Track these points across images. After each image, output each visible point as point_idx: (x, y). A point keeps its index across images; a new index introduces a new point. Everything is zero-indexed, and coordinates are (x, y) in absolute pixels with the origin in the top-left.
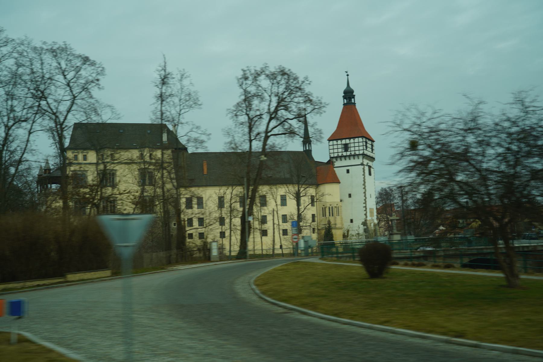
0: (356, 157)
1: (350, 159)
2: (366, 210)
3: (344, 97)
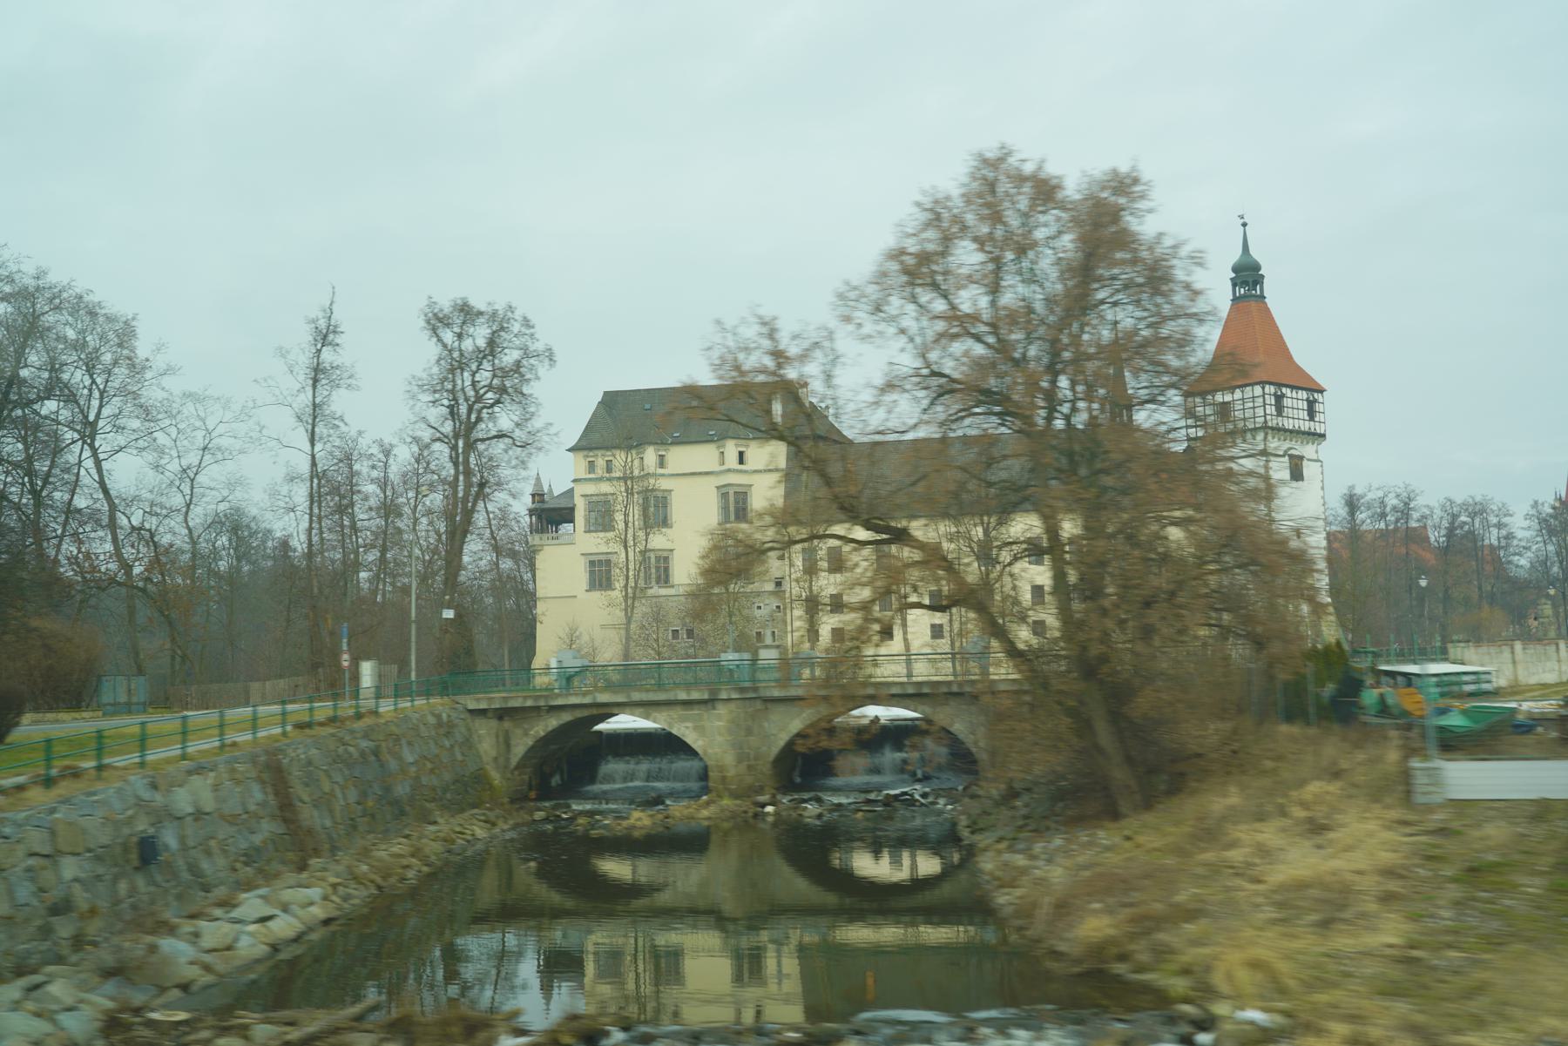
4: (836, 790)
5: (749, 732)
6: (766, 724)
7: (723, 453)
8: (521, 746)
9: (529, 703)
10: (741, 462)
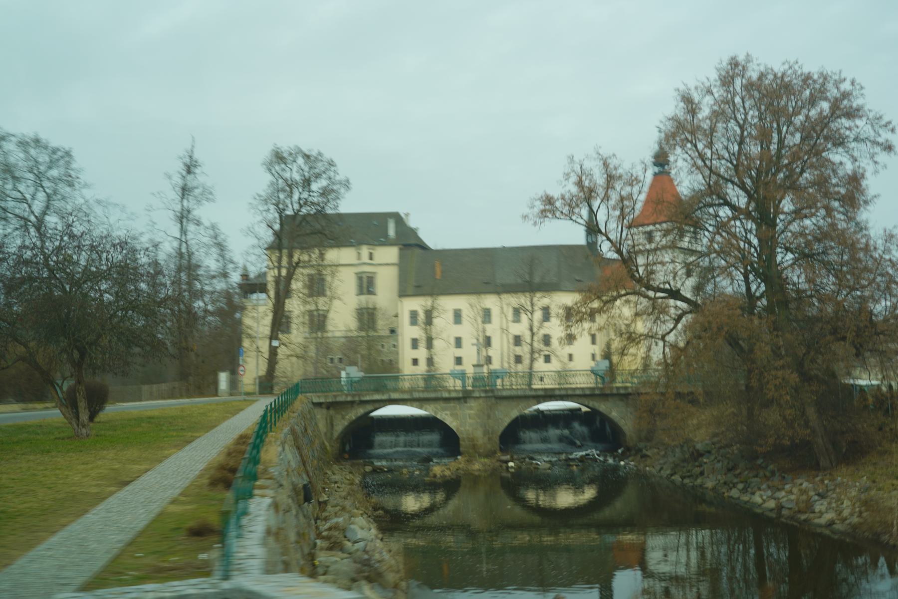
4: (380, 457)
5: (489, 417)
6: (497, 413)
8: (340, 426)
9: (349, 399)
10: (371, 258)
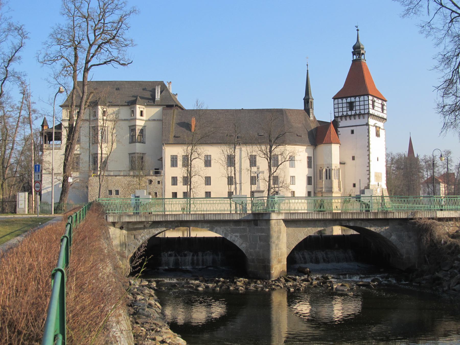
0: (361, 116)
1: (351, 119)
2: (369, 174)
3: (354, 54)
7: (133, 111)
